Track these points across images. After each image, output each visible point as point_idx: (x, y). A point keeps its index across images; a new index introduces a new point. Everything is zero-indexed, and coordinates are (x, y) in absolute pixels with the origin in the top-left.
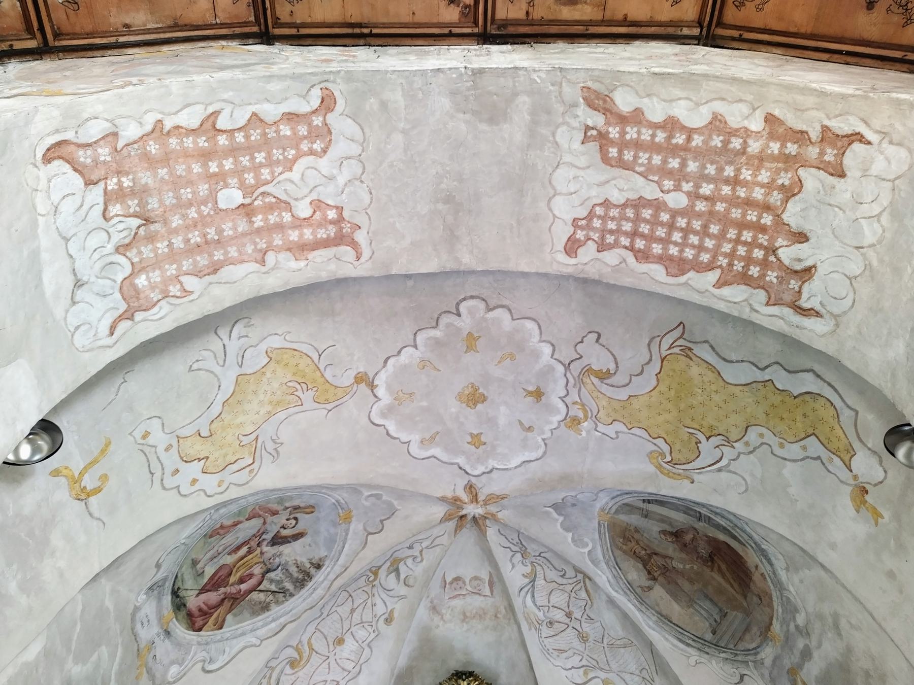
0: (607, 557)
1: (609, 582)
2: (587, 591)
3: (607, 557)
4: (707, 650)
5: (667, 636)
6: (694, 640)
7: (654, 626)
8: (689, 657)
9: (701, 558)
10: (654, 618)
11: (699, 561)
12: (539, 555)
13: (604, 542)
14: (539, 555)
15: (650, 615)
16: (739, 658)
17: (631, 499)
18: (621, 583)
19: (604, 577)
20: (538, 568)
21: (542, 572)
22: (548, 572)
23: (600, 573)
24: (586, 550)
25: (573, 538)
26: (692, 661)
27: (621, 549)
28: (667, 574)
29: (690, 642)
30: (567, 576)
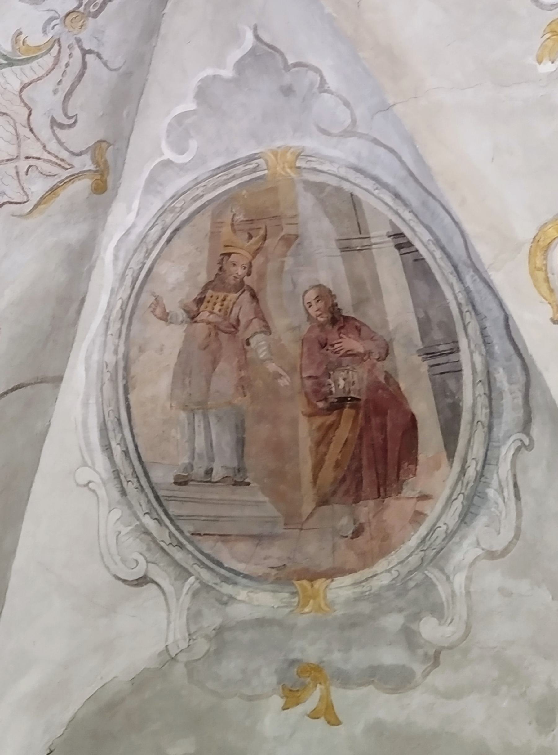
0: (178, 205)
1: (128, 233)
2: (53, 191)
3: (178, 205)
4: (131, 488)
5: (92, 401)
6: (126, 453)
7: (94, 367)
8: (85, 464)
9: (321, 385)
10: (110, 358)
11: (309, 383)
12: (85, 53)
13: (211, 183)
14: (85, 53)
15: (111, 347)
16: (178, 555)
17: (381, 208)
18: (140, 256)
19: (131, 218)
20: (48, 60)
21: (41, 73)
22: (48, 85)
23: (136, 205)
24: (168, 154)
25: (185, 115)
26: (85, 475)
27: (216, 224)
28: (223, 337)
29: (117, 450)
30: (62, 134)
